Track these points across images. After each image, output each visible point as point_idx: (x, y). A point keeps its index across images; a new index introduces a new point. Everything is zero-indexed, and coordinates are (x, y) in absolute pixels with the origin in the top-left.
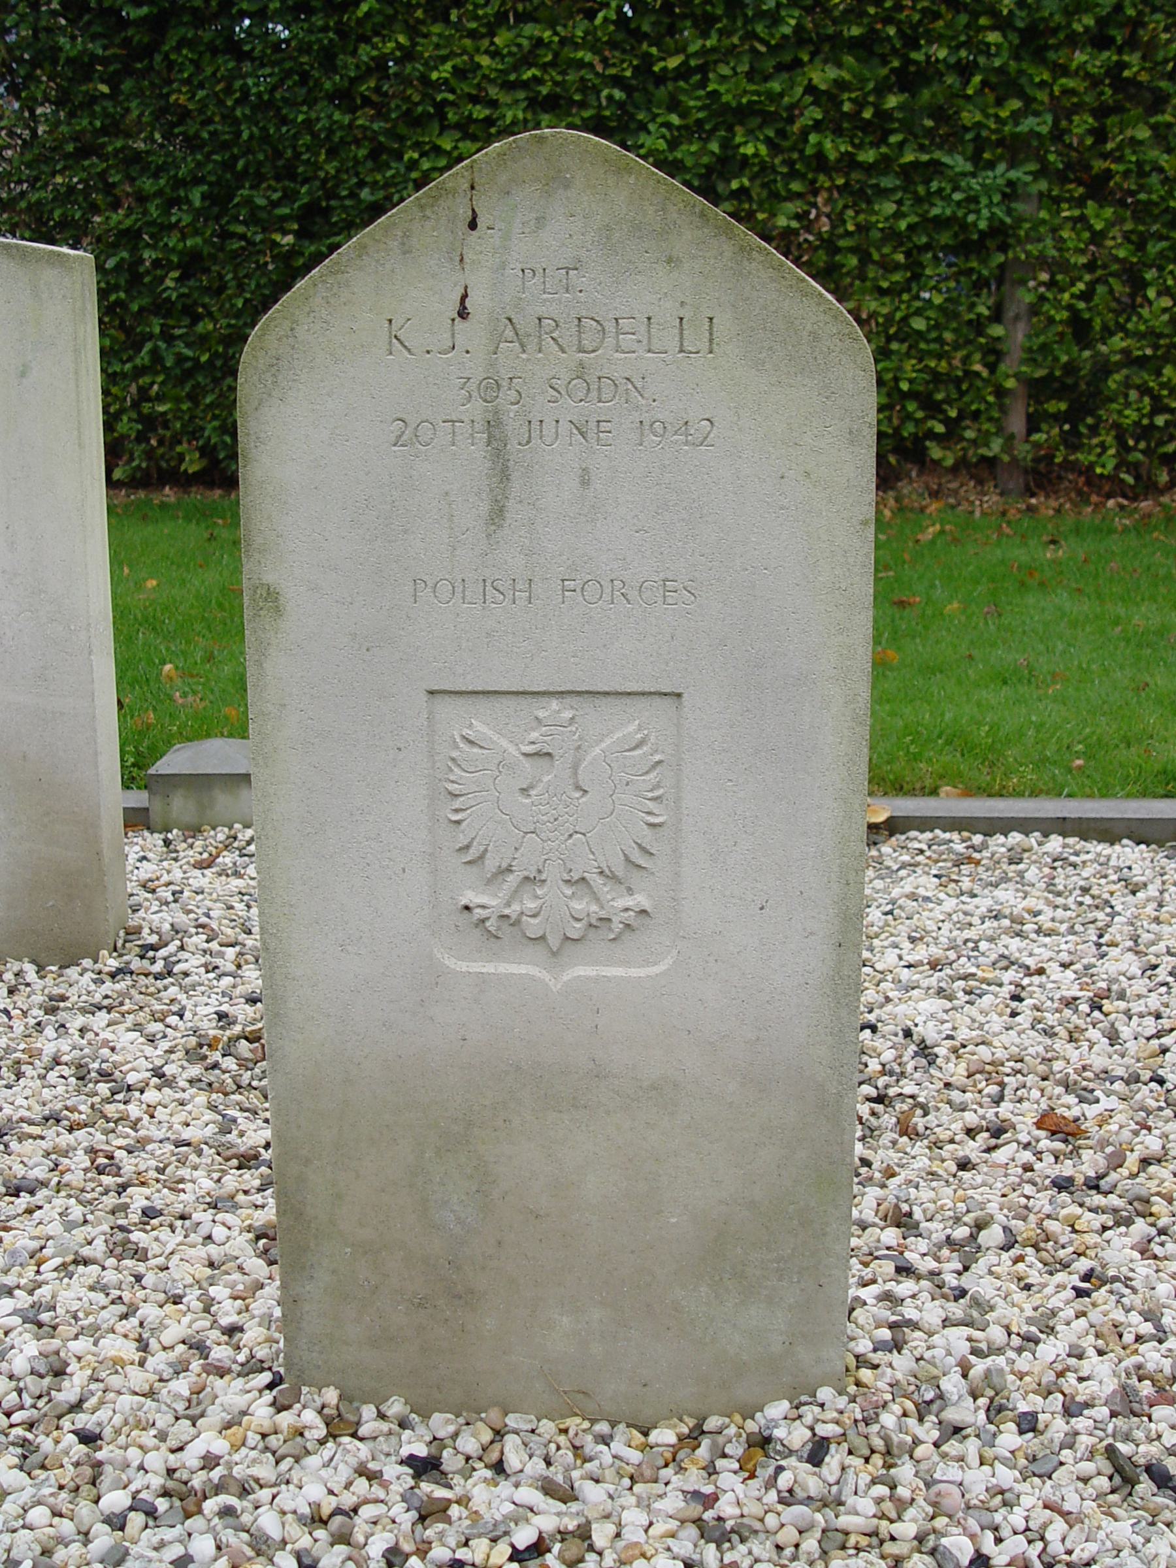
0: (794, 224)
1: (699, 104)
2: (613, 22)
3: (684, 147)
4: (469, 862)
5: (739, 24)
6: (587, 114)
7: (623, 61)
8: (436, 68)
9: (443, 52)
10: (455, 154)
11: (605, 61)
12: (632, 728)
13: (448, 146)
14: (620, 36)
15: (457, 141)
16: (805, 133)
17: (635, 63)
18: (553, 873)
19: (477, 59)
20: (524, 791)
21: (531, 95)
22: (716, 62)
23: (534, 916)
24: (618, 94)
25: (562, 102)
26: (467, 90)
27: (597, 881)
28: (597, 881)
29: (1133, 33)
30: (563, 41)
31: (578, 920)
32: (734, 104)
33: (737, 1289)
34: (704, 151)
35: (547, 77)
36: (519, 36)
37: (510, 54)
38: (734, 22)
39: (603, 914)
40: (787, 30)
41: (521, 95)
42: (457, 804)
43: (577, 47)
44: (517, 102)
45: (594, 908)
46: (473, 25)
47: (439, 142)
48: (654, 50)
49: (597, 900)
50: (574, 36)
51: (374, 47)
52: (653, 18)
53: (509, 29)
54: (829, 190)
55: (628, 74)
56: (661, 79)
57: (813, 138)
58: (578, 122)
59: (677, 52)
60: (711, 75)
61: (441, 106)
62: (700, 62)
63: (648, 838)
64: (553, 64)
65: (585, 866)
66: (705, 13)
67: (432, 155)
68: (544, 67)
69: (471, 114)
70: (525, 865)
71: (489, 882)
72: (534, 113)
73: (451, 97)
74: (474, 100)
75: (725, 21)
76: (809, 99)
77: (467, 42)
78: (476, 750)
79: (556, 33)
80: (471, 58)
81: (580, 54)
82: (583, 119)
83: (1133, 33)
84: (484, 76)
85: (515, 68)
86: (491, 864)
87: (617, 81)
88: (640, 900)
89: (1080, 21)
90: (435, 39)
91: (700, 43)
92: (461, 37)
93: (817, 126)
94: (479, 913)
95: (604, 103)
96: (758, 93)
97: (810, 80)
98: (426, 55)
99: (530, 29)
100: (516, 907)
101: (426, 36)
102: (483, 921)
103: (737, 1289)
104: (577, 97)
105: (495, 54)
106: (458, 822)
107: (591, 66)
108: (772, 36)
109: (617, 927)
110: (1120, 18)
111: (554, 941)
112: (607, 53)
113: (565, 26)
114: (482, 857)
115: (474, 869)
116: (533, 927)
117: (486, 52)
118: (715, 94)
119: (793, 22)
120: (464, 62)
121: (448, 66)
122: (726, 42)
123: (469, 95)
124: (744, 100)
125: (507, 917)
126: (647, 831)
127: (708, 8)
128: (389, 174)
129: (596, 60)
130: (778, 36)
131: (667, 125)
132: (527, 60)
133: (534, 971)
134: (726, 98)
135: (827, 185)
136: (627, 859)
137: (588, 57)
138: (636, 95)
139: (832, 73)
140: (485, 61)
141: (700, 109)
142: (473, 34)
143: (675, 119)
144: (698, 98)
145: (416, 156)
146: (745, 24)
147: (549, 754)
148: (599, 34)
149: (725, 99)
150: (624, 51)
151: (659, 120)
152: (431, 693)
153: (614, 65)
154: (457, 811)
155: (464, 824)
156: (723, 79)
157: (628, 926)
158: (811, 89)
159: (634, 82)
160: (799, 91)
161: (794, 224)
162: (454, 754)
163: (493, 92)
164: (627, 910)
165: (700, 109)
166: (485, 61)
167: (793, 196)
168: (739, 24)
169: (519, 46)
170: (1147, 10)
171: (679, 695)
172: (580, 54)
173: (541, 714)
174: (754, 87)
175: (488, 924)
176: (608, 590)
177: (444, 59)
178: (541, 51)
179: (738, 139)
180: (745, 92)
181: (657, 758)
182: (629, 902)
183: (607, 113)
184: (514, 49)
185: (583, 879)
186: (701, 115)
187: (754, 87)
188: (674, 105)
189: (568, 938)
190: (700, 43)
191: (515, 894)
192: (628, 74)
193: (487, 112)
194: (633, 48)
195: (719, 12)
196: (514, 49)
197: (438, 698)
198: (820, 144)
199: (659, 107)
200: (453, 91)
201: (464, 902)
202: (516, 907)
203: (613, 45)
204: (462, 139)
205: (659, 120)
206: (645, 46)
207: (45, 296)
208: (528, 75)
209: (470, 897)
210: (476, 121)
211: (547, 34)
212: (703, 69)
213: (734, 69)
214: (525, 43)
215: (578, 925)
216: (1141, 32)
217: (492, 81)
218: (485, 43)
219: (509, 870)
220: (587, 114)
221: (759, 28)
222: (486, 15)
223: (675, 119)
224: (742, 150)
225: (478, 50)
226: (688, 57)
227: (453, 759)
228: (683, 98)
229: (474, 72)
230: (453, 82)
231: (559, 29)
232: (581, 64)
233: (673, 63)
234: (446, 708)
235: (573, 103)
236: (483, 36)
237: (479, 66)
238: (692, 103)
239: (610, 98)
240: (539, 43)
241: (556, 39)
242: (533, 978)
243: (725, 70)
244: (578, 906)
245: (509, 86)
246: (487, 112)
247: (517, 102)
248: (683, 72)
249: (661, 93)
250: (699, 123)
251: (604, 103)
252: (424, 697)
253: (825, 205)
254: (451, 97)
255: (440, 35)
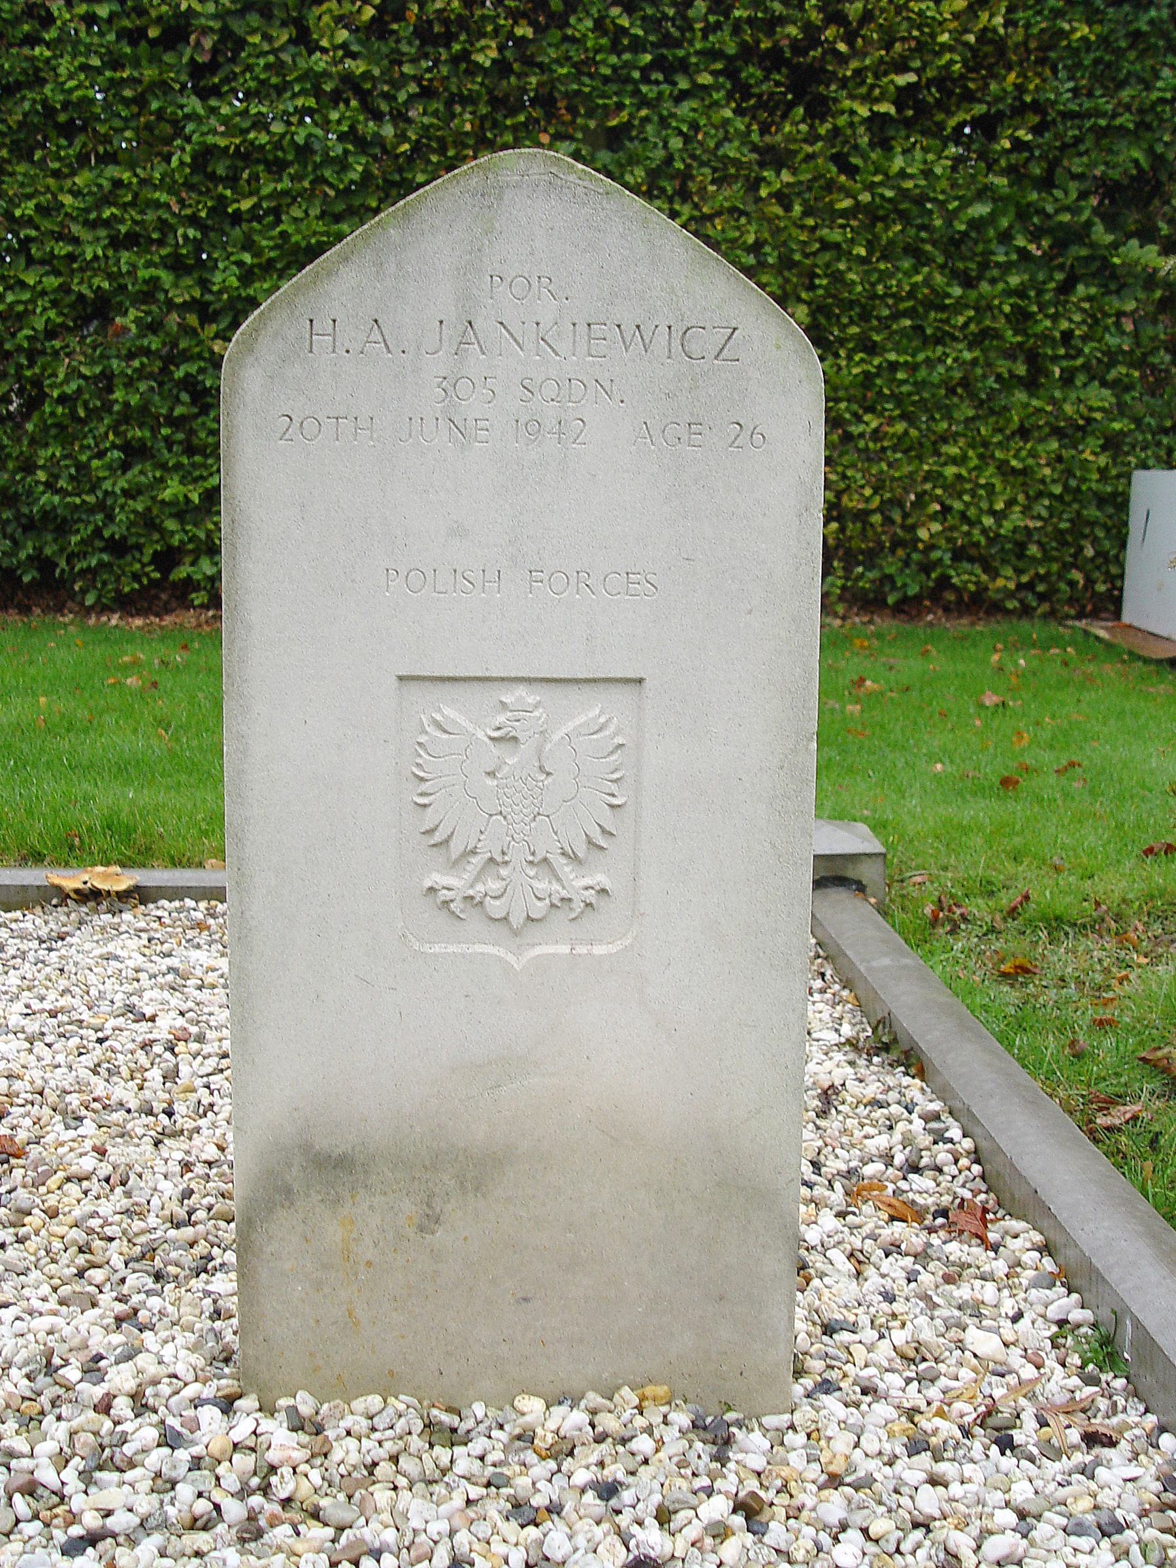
1: (271, 243)
2: (189, 166)
3: (257, 285)
4: (434, 845)
5: (310, 169)
6: (164, 252)
7: (199, 202)
8: (19, 206)
9: (28, 190)
10: (39, 288)
11: (182, 202)
14: (195, 179)
17: (209, 204)
18: (518, 854)
20: (491, 774)
21: (113, 232)
22: (289, 205)
24: (191, 233)
25: (142, 240)
26: (49, 226)
27: (559, 861)
28: (559, 861)
29: (683, 185)
30: (143, 182)
32: (303, 244)
35: (127, 217)
36: (99, 176)
37: (90, 193)
38: (305, 167)
39: (564, 894)
40: (355, 176)
41: (102, 233)
42: (424, 787)
43: (155, 188)
44: (98, 239)
45: (556, 886)
46: (55, 165)
47: (22, 277)
48: (228, 193)
49: (559, 880)
50: (151, 178)
52: (228, 163)
53: (91, 169)
55: (203, 214)
56: (237, 218)
58: (156, 259)
59: (251, 194)
60: (284, 217)
61: (26, 242)
62: (273, 204)
63: (608, 819)
64: (133, 204)
65: (547, 846)
66: (276, 158)
67: (17, 289)
68: (125, 207)
69: (52, 249)
70: (489, 847)
72: (116, 251)
73: (33, 233)
74: (60, 237)
75: (296, 166)
77: (51, 181)
78: (445, 736)
79: (136, 175)
80: (55, 196)
81: (157, 195)
82: (161, 257)
83: (683, 185)
84: (67, 214)
85: (98, 206)
87: (193, 221)
88: (600, 879)
89: (632, 173)
90: (20, 178)
91: (272, 186)
92: (45, 177)
94: (445, 894)
95: (181, 241)
96: (327, 234)
98: (11, 193)
99: (112, 171)
100: (480, 887)
101: (11, 175)
104: (155, 236)
105: (76, 193)
106: (425, 806)
108: (342, 181)
109: (578, 906)
110: (671, 171)
112: (184, 195)
113: (144, 168)
114: (446, 842)
115: (443, 850)
116: (496, 908)
117: (70, 192)
118: (284, 234)
119: (360, 168)
120: (48, 201)
121: (31, 204)
122: (298, 186)
123: (53, 232)
124: (313, 241)
125: (472, 898)
127: (280, 154)
129: (173, 201)
130: (346, 181)
131: (240, 264)
132: (106, 200)
134: (296, 238)
136: (590, 842)
137: (163, 197)
138: (212, 234)
140: (67, 200)
141: (272, 249)
142: (56, 174)
143: (247, 258)
144: (271, 238)
146: (314, 170)
147: (515, 739)
148: (177, 176)
149: (294, 239)
150: (201, 193)
151: (232, 259)
152: (401, 678)
153: (190, 206)
154: (421, 795)
155: (430, 810)
159: (210, 222)
162: (423, 739)
163: (76, 229)
165: (272, 249)
166: (67, 200)
168: (310, 169)
169: (100, 186)
170: (695, 164)
171: (640, 681)
176: (573, 581)
177: (29, 197)
178: (121, 192)
180: (315, 233)
181: (619, 740)
182: (588, 881)
183: (184, 251)
184: (95, 189)
185: (545, 860)
186: (273, 254)
188: (248, 245)
190: (272, 186)
191: (477, 879)
192: (203, 214)
193: (70, 248)
194: (208, 190)
195: (290, 157)
196: (95, 189)
197: (413, 687)
199: (234, 246)
200: (37, 228)
201: (428, 883)
202: (480, 887)
203: (190, 187)
204: (47, 274)
205: (232, 259)
206: (220, 188)
208: (106, 214)
209: (438, 878)
210: (59, 257)
211: (126, 176)
212: (276, 212)
213: (306, 212)
214: (105, 183)
215: (539, 904)
216: (690, 184)
217: (73, 219)
218: (68, 183)
219: (473, 852)
220: (164, 252)
221: (327, 173)
222: (68, 156)
223: (247, 258)
225: (61, 189)
226: (261, 199)
227: (420, 744)
228: (256, 238)
229: (58, 210)
230: (37, 219)
231: (138, 171)
232: (158, 205)
233: (246, 205)
235: (152, 241)
236: (66, 176)
237: (63, 205)
238: (264, 243)
239: (185, 237)
240: (117, 183)
243: (297, 212)
244: (541, 886)
245: (92, 225)
246: (70, 248)
247: (98, 239)
248: (254, 215)
249: (237, 233)
250: (271, 262)
251: (181, 241)
252: (396, 683)
254: (33, 233)
255: (25, 175)
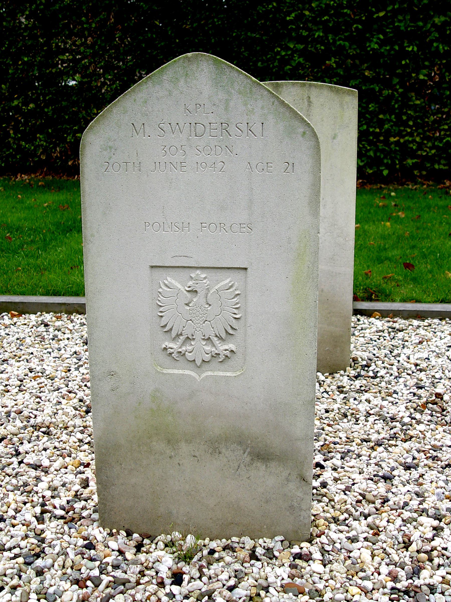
0: (426, 78)
4: (165, 332)
9: (291, 9)
12: (228, 280)
13: (292, 46)
15: (295, 44)
16: (432, 41)
18: (198, 336)
19: (304, 12)
20: (187, 305)
23: (190, 352)
31: (207, 354)
33: (265, 487)
34: (392, 49)
39: (217, 352)
42: (161, 309)
45: (214, 349)
51: (264, 7)
54: (439, 65)
57: (435, 45)
58: (343, 37)
60: (396, 20)
63: (235, 324)
65: (210, 333)
70: (187, 332)
71: (174, 339)
76: (433, 29)
81: (345, 11)
86: (174, 333)
88: (232, 346)
93: (437, 40)
97: (434, 21)
102: (171, 354)
103: (265, 487)
106: (162, 316)
107: (349, 16)
111: (198, 362)
114: (171, 329)
116: (189, 356)
124: (409, 29)
125: (181, 352)
126: (234, 321)
128: (269, 56)
131: (379, 38)
133: (187, 372)
135: (439, 62)
136: (227, 332)
139: (443, 19)
140: (307, 13)
141: (390, 33)
145: (279, 49)
147: (196, 291)
152: (152, 267)
154: (161, 312)
156: (400, 21)
157: (227, 356)
158: (434, 25)
160: (429, 26)
161: (426, 78)
162: (160, 290)
164: (226, 350)
165: (390, 33)
166: (307, 13)
167: (425, 67)
169: (321, 7)
171: (246, 269)
172: (345, 11)
173: (193, 275)
174: (412, 24)
175: (173, 355)
179: (406, 45)
182: (226, 347)
187: (412, 24)
189: (204, 361)
191: (184, 344)
197: (153, 269)
198: (438, 47)
202: (184, 348)
207: (345, 107)
219: (181, 335)
223: (381, 37)
224: (407, 49)
227: (159, 292)
234: (157, 272)
238: (388, 30)
241: (335, 5)
242: (190, 375)
243: (400, 18)
253: (437, 70)
